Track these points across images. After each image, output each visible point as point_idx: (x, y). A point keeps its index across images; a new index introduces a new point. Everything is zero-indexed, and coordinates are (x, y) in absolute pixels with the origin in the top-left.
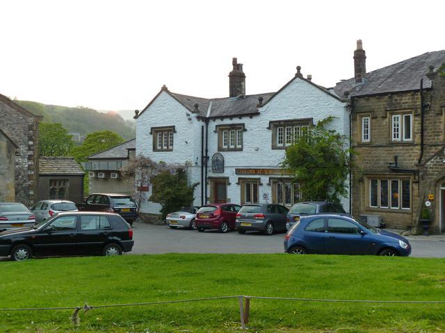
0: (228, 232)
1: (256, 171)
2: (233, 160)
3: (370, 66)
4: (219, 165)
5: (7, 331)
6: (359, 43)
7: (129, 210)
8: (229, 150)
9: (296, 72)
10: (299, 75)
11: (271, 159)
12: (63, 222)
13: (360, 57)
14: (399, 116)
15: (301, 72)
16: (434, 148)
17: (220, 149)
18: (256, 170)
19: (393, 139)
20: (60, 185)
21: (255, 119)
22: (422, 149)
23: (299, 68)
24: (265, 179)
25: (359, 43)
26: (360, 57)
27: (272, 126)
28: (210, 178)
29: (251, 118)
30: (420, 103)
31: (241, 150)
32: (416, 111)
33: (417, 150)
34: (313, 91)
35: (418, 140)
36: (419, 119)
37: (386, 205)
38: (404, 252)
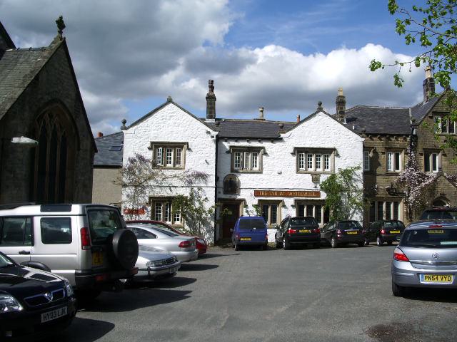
1: (278, 193)
2: (249, 185)
5: (208, 340)
11: (295, 182)
17: (232, 170)
18: (279, 192)
21: (278, 144)
24: (289, 202)
31: (260, 172)
38: (184, 334)
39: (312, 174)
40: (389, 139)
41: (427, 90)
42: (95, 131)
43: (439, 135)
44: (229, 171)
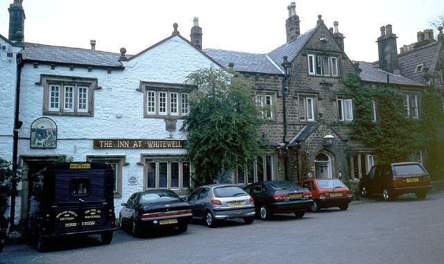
0: (388, 200)
1: (115, 143)
7: (417, 180)
8: (63, 114)
9: (172, 30)
10: (176, 33)
11: (143, 130)
15: (178, 29)
16: (292, 127)
19: (65, 109)
21: (115, 76)
22: (285, 127)
23: (176, 26)
24: (134, 156)
27: (44, 80)
28: (24, 158)
29: (109, 72)
30: (281, 87)
31: (90, 114)
32: (278, 94)
33: (280, 128)
34: (196, 55)
35: (280, 119)
39: (165, 118)
40: (371, 85)
41: (291, 29)
42: (417, 41)
43: (312, 76)
44: (41, 112)
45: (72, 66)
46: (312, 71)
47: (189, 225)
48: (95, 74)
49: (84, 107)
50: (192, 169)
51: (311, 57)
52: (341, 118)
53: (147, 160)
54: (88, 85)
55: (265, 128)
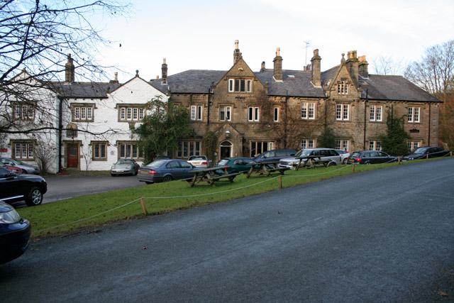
3: (169, 73)
4: (73, 132)
6: (165, 60)
10: (137, 76)
12: (195, 163)
13: (165, 68)
14: (195, 107)
20: (310, 146)
23: (137, 71)
25: (165, 60)
26: (165, 68)
28: (64, 141)
36: (207, 109)
37: (98, 156)
39: (129, 122)
45: (84, 98)
46: (231, 90)
47: (82, 170)
48: (95, 101)
49: (312, 116)
50: (334, 159)
51: (231, 81)
52: (200, 118)
53: (119, 144)
54: (91, 106)
55: (196, 125)
